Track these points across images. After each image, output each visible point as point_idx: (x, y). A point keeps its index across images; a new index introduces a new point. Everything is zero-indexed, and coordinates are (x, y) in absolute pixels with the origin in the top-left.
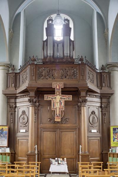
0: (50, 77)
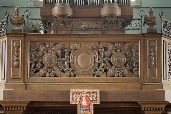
0: (63, 71)
